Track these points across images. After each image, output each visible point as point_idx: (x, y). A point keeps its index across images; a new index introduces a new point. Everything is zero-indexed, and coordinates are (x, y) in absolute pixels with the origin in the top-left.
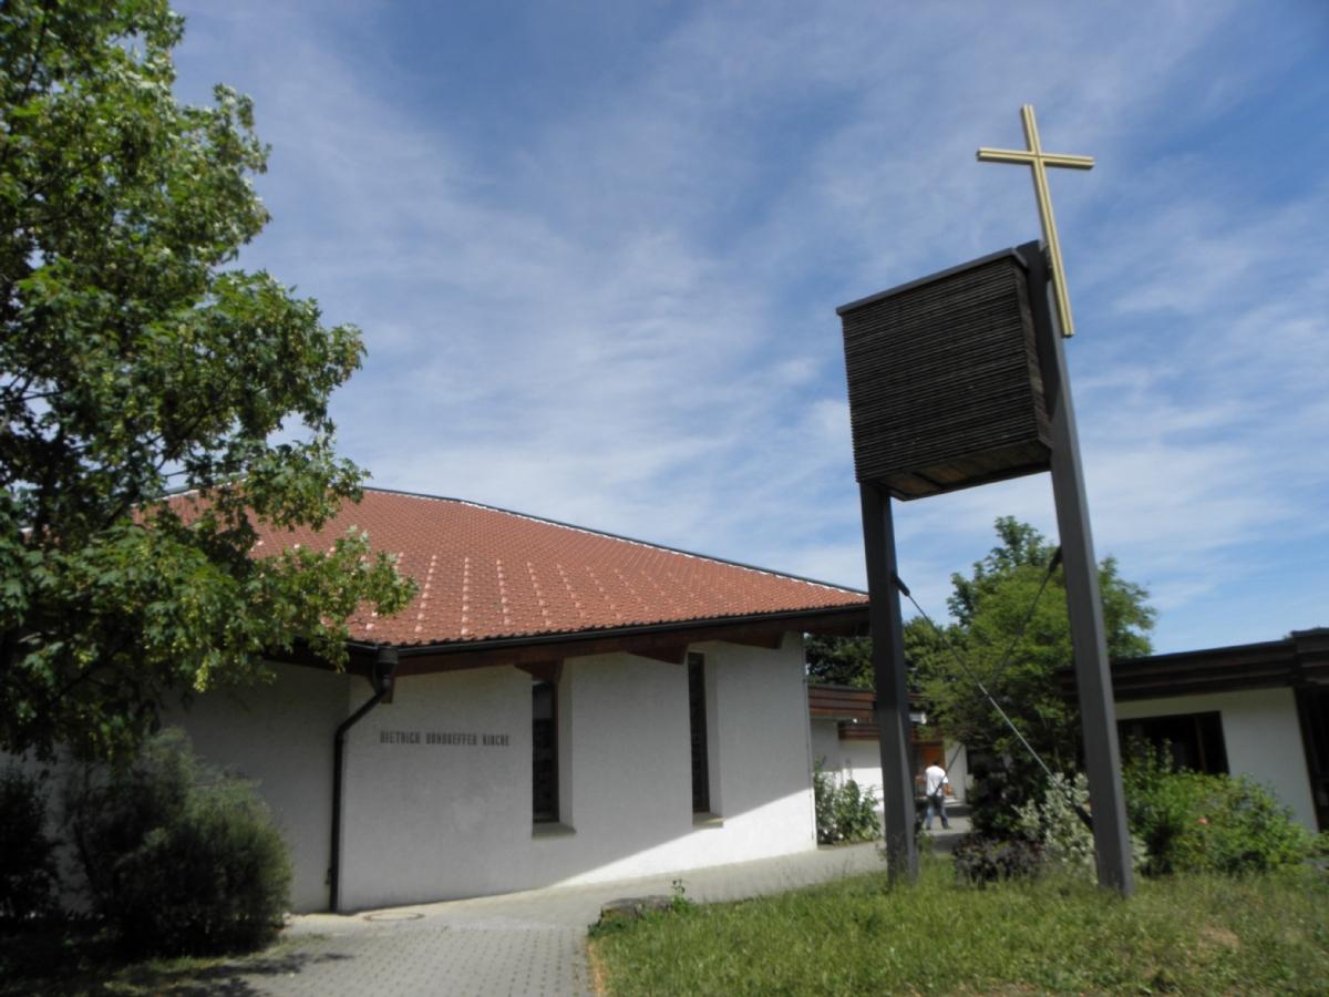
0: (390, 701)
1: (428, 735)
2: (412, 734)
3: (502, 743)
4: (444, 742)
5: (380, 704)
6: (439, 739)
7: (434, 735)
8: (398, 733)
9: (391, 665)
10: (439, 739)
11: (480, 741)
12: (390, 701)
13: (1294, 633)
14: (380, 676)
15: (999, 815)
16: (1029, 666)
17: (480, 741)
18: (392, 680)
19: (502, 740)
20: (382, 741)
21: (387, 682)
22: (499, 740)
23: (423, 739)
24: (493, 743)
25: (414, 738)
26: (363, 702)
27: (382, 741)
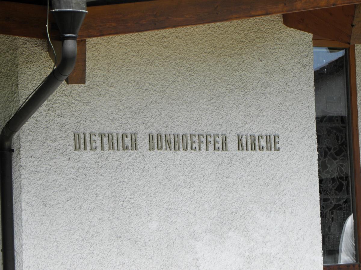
0: (81, 79)
1: (151, 137)
2: (124, 135)
3: (269, 148)
4: (178, 149)
5: (63, 87)
6: (168, 142)
7: (159, 136)
8: (101, 135)
9: (75, 15)
10: (176, 143)
11: (233, 145)
12: (81, 79)
13: (2, 251)
14: (59, 38)
15: (333, 229)
16: (216, 201)
17: (233, 145)
18: (82, 44)
19: (268, 142)
20: (77, 148)
21: (71, 45)
22: (263, 143)
23: (143, 143)
24: (253, 148)
25: (128, 141)
26: (37, 82)
27: (77, 148)
